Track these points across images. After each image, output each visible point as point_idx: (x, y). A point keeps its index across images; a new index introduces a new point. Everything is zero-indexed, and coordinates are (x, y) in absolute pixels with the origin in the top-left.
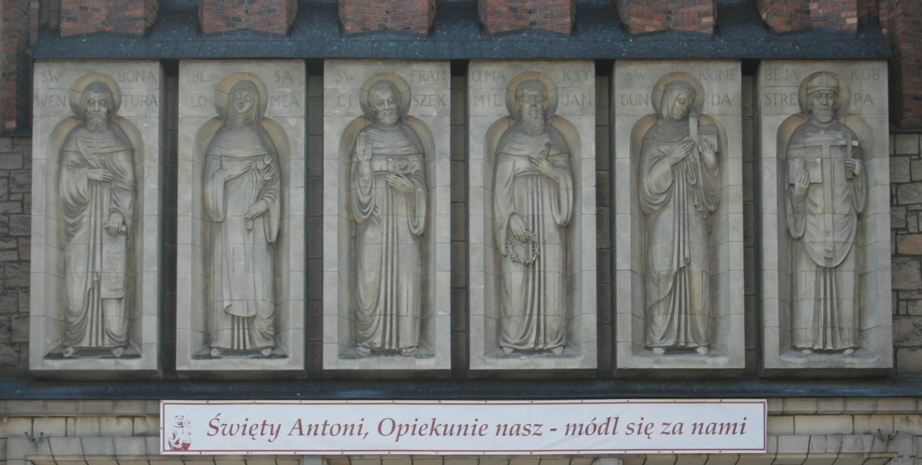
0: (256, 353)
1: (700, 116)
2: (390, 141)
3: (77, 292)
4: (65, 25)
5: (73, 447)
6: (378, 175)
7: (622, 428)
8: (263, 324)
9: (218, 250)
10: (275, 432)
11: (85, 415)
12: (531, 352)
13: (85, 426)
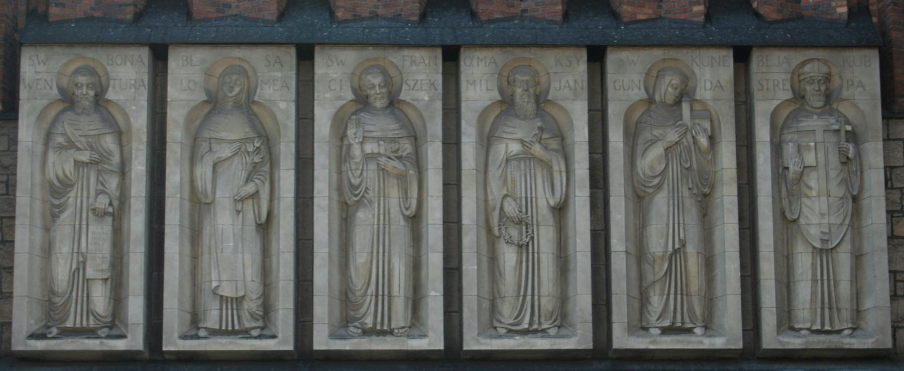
0: (245, 333)
1: (693, 101)
2: (381, 125)
8: (252, 305)
9: (207, 230)
12: (525, 332)
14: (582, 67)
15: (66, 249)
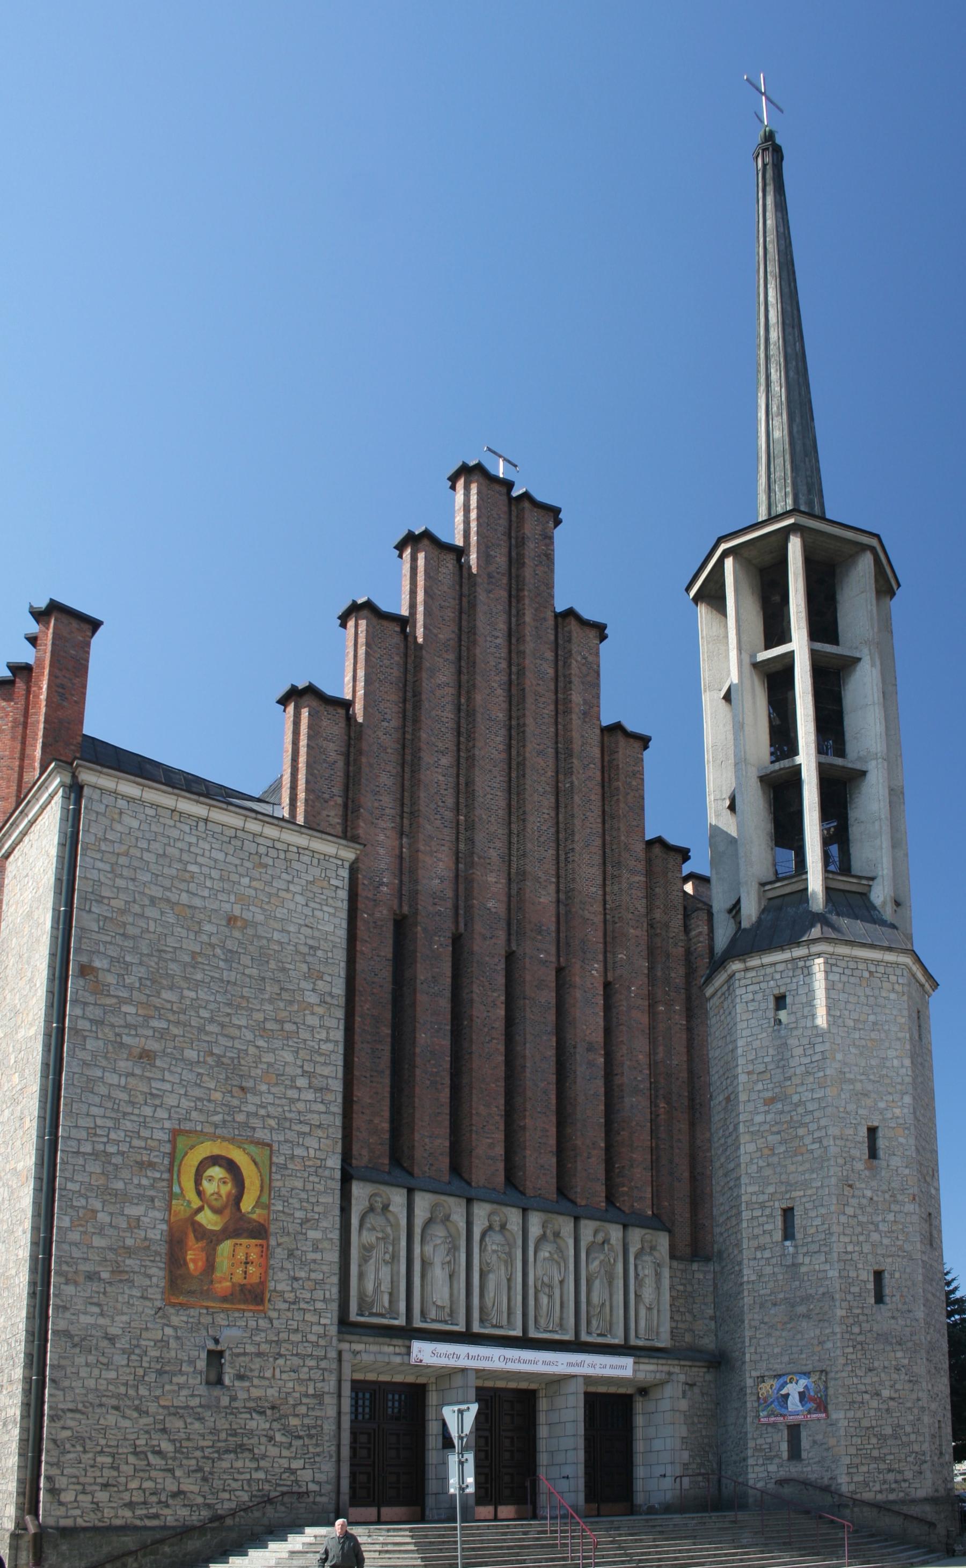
0: (446, 1322)
1: (609, 1244)
2: (498, 1238)
3: (370, 1287)
4: (354, 1161)
5: (372, 1358)
6: (494, 1251)
7: (586, 1365)
8: (447, 1310)
9: (429, 1276)
10: (458, 1358)
11: (374, 1343)
12: (550, 1331)
13: (374, 1348)
14: (572, 1225)
15: (373, 1277)
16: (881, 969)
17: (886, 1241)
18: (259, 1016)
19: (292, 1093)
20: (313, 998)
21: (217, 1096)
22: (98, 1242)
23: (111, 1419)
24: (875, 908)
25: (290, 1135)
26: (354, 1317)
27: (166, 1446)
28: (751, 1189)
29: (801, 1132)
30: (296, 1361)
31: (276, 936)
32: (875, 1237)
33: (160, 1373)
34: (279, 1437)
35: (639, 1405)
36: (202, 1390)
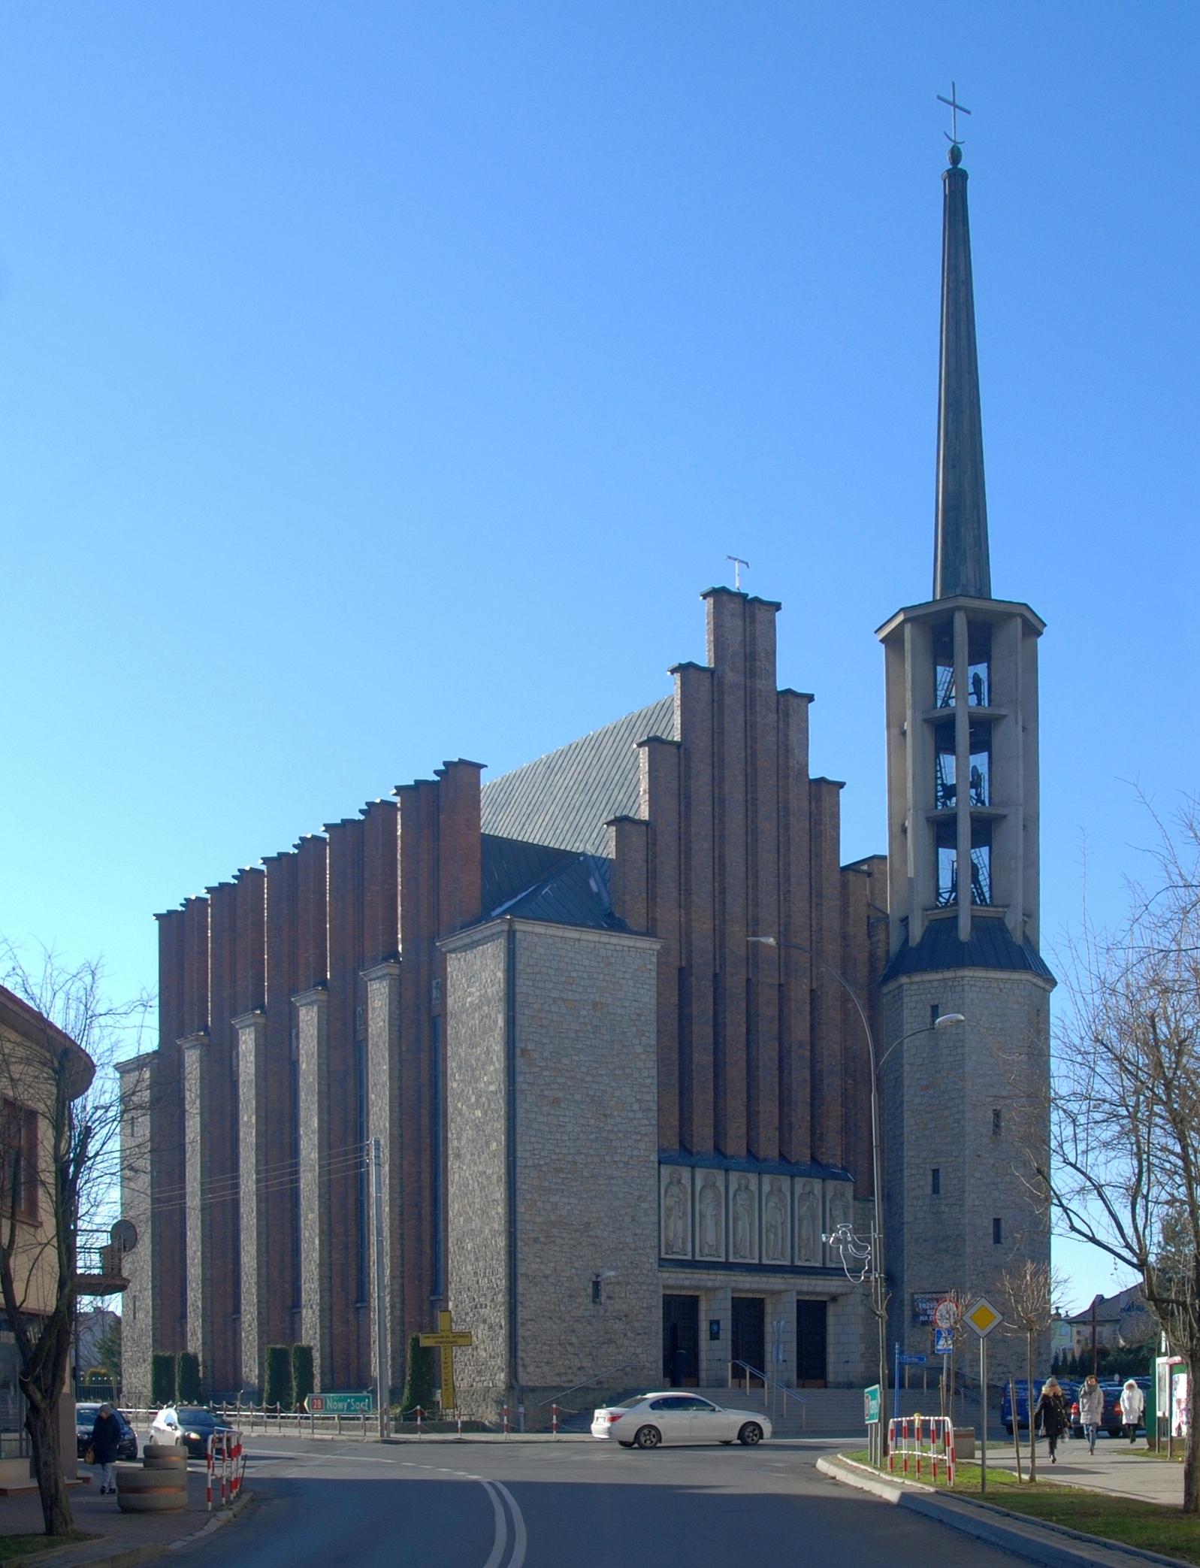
16: (1008, 986)
17: (1003, 1197)
18: (611, 1066)
19: (631, 1115)
20: (639, 1050)
21: (592, 1122)
22: (538, 1219)
23: (549, 1323)
24: (1008, 931)
25: (630, 1142)
26: (663, 1256)
27: (574, 1340)
28: (911, 1153)
29: (946, 1113)
30: (637, 1287)
31: (619, 1011)
32: (996, 1193)
33: (571, 1296)
34: (629, 1334)
35: (831, 1310)
36: (591, 1306)
